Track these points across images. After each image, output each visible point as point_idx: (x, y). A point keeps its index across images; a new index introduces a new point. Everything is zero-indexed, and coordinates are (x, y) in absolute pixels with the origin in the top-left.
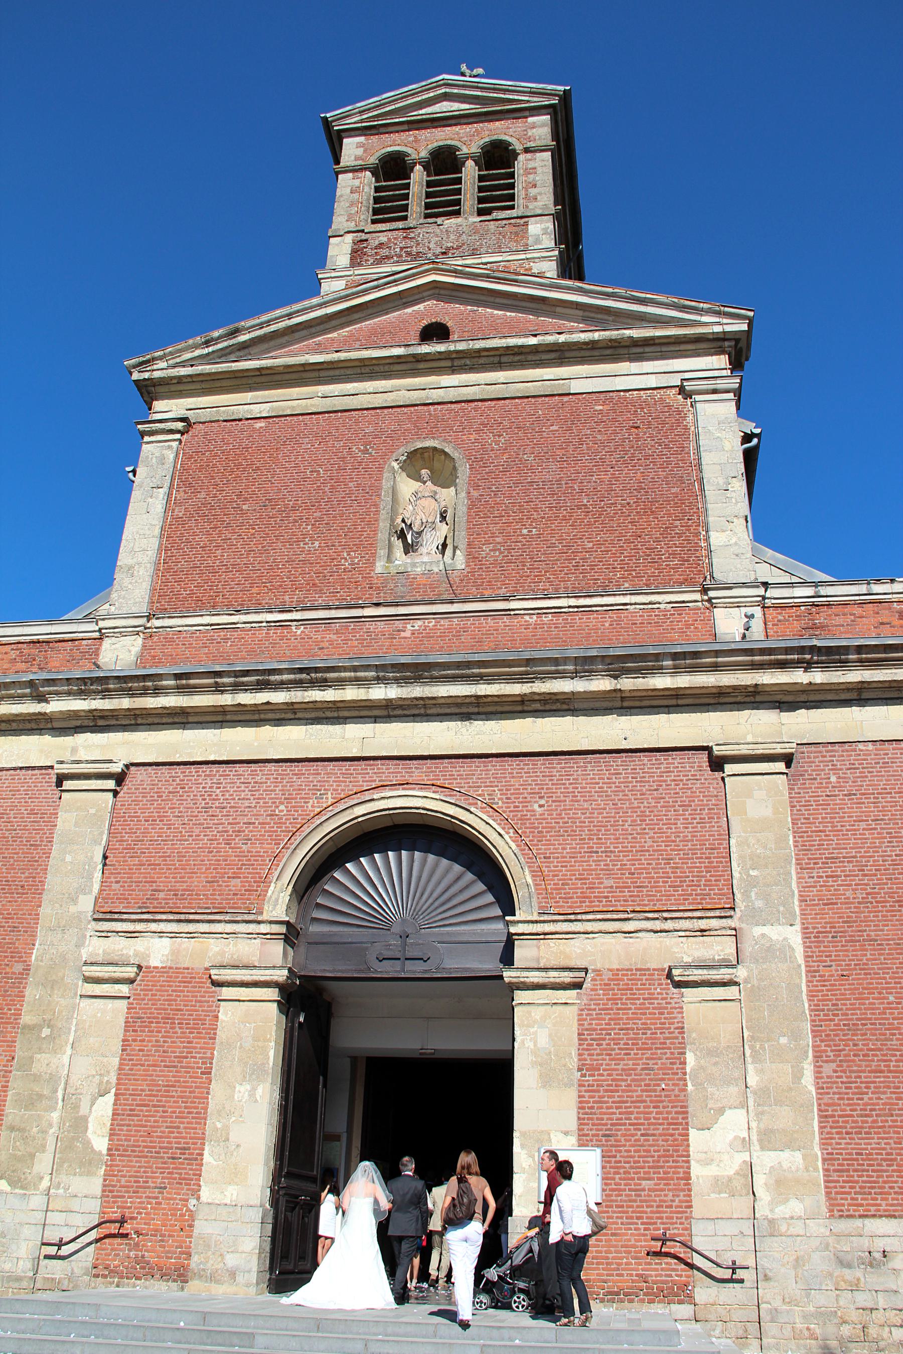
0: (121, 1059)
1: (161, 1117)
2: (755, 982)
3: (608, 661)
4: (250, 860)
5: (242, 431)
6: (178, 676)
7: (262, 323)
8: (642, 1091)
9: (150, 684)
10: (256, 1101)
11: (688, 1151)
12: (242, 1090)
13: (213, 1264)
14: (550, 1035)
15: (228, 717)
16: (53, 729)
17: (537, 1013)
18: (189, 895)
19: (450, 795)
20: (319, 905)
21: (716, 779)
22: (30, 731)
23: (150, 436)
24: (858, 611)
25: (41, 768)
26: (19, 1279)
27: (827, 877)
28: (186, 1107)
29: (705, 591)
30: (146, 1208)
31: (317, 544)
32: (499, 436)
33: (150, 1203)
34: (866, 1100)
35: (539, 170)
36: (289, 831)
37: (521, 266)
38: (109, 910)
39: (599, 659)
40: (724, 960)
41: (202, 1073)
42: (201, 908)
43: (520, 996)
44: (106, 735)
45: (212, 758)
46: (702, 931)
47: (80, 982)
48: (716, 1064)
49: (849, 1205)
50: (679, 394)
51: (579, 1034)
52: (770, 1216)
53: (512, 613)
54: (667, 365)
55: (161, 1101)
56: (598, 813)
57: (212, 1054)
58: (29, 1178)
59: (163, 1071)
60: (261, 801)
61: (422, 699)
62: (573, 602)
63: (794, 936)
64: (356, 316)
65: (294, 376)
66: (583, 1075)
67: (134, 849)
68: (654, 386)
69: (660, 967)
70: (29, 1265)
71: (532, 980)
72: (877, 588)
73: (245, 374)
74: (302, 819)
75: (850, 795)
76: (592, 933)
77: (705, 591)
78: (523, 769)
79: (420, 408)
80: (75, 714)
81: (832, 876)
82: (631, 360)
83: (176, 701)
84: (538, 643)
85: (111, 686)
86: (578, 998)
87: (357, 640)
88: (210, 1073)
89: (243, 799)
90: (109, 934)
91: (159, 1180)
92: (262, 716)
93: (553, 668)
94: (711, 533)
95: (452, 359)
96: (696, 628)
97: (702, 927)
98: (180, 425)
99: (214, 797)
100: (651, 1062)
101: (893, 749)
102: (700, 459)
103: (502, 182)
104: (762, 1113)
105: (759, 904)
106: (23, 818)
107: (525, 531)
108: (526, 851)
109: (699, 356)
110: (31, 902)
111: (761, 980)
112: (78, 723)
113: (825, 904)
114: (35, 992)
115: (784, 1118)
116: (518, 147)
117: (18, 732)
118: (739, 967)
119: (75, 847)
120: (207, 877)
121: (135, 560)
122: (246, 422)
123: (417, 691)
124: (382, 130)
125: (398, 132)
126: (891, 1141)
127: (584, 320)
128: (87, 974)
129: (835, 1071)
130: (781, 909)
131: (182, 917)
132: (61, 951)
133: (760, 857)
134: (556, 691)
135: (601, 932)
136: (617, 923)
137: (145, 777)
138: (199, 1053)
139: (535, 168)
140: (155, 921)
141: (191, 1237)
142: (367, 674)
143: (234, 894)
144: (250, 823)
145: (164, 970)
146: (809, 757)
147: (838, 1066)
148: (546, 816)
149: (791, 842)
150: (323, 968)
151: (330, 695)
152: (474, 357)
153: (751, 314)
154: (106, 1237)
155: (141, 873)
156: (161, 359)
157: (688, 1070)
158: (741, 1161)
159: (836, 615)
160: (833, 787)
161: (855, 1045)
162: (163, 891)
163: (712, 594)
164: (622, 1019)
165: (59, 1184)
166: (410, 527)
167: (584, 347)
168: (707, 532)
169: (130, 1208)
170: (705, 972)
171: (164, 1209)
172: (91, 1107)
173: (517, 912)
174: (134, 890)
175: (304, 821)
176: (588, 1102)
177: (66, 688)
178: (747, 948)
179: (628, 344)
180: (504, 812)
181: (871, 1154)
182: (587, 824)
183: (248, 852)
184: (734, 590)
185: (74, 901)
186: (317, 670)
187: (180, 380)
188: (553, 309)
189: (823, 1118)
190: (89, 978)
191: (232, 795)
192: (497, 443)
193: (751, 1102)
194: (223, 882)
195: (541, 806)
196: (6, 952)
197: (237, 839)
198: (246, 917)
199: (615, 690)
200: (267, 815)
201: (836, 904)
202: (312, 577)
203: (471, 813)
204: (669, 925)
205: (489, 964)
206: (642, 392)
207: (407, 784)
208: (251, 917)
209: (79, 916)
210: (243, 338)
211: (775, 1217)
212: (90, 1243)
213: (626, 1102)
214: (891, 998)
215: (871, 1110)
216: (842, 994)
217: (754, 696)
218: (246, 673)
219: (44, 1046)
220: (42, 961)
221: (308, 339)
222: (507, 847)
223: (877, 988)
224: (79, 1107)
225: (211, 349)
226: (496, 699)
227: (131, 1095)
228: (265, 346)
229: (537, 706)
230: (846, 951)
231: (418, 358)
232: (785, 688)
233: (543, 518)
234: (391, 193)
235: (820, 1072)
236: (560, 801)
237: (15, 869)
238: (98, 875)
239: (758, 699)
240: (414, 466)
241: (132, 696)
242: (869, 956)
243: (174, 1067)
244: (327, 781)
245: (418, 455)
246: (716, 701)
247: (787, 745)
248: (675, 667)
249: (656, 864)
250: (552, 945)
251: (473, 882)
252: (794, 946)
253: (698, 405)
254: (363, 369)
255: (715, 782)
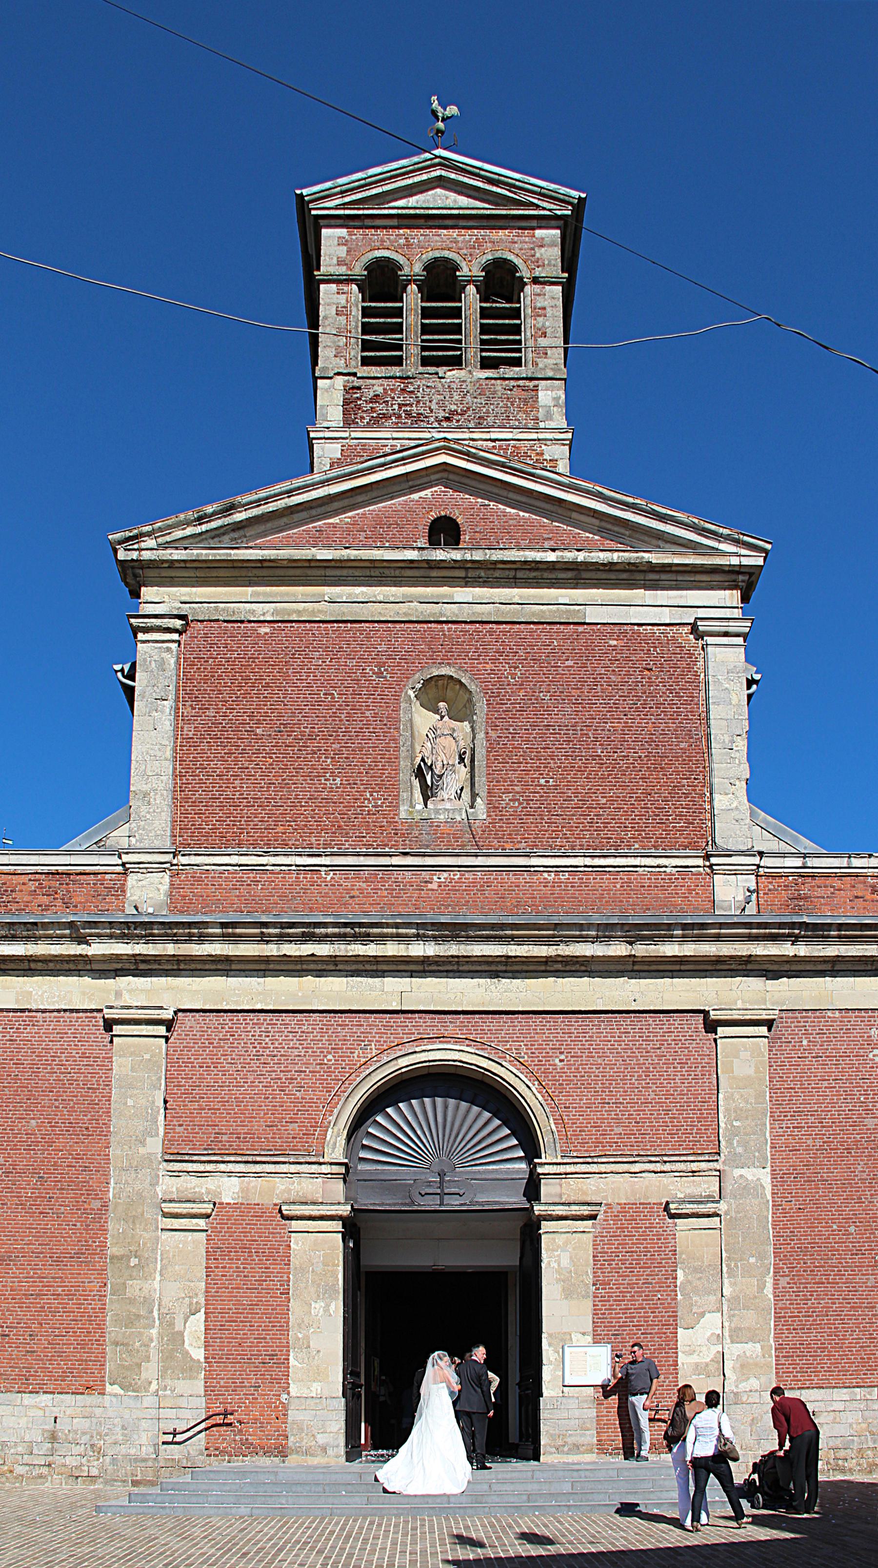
0: (206, 1284)
1: (249, 1330)
2: (733, 1214)
3: (626, 928)
4: (304, 1106)
5: (245, 636)
6: (223, 925)
7: (259, 500)
8: (643, 1300)
9: (196, 931)
10: (330, 1315)
11: (676, 1345)
12: (318, 1307)
13: (306, 1442)
14: (571, 1258)
15: (271, 966)
16: (92, 970)
17: (560, 1239)
18: (250, 1138)
19: (482, 1049)
20: (364, 1147)
21: (709, 1040)
22: (68, 973)
23: (144, 632)
24: (837, 883)
25: (85, 1011)
26: (145, 1460)
27: (794, 1127)
28: (270, 1322)
29: (707, 857)
30: (245, 1403)
31: (338, 780)
32: (515, 668)
33: (248, 1399)
34: (809, 1304)
35: (549, 312)
36: (339, 1080)
37: (531, 449)
38: (176, 1151)
39: (619, 926)
40: (709, 1196)
41: (281, 1293)
42: (264, 1150)
43: (546, 1226)
44: (149, 979)
45: (258, 1007)
46: (693, 1172)
47: (160, 1217)
48: (700, 1279)
49: (792, 1380)
50: (691, 633)
51: (594, 1256)
52: (735, 1390)
53: (532, 869)
54: (681, 597)
55: (247, 1317)
56: (610, 1069)
57: (288, 1277)
58: (139, 1383)
59: (246, 1293)
60: (310, 1050)
61: (458, 957)
62: (588, 861)
63: (765, 1177)
64: (360, 499)
65: (298, 572)
66: (598, 1289)
67: (192, 1094)
68: (668, 621)
69: (659, 1201)
70: (152, 1450)
71: (557, 1213)
72: (856, 862)
73: (245, 565)
74: (350, 1068)
75: (817, 1057)
76: (605, 1173)
77: (707, 857)
78: (545, 1026)
79: (433, 625)
80: (117, 958)
81: (797, 1127)
82: (646, 588)
83: (222, 949)
84: (556, 902)
85: (156, 931)
86: (593, 1228)
87: (386, 889)
88: (288, 1293)
89: (293, 1048)
90: (181, 1174)
91: (253, 1381)
92: (305, 967)
93: (578, 933)
94: (716, 796)
95: (467, 569)
96: (697, 893)
97: (694, 1169)
98: (178, 623)
99: (263, 1045)
100: (650, 1278)
101: (856, 1017)
102: (708, 712)
103: (507, 322)
104: (733, 1316)
105: (740, 1150)
106: (75, 1061)
107: (542, 781)
108: (549, 1102)
109: (712, 588)
110: (98, 1143)
111: (738, 1212)
112: (119, 966)
113: (790, 1151)
114: (117, 1226)
115: (750, 1318)
116: (525, 273)
117: (55, 973)
118: (722, 1202)
119: (136, 1092)
120: (266, 1122)
121: (149, 785)
122: (249, 625)
123: (453, 949)
124: (368, 222)
125: (385, 227)
126: (825, 1334)
127: (599, 531)
128: (165, 1210)
129: (789, 1283)
130: (757, 1154)
131: (250, 1159)
132: (136, 1189)
133: (742, 1110)
134: (578, 954)
135: (612, 1172)
136: (626, 1165)
137: (193, 1023)
138: (277, 1277)
139: (544, 308)
140: (223, 1162)
141: (286, 1423)
142: (408, 931)
143: (293, 1138)
144: (301, 1071)
145: (236, 1206)
146: (786, 1022)
147: (791, 1279)
148: (566, 1070)
149: (768, 1098)
150: (372, 1202)
151: (371, 950)
152: (489, 569)
153: (769, 547)
154: (213, 1426)
155: (202, 1117)
156: (149, 536)
157: (678, 1284)
158: (715, 1352)
159: (819, 887)
160: (804, 1050)
161: (805, 1263)
162: (226, 1134)
163: (714, 860)
164: (628, 1244)
165: (166, 1387)
166: (430, 768)
167: (602, 568)
168: (711, 794)
169: (230, 1403)
170: (696, 1206)
171: (260, 1403)
172: (185, 1323)
173: (543, 1155)
174: (198, 1133)
175: (352, 1071)
176: (601, 1310)
177: (108, 931)
178: (728, 1187)
179: (645, 568)
180: (530, 1065)
181: (810, 1344)
182: (600, 1078)
183: (303, 1098)
184: (733, 858)
185: (143, 1143)
186: (361, 925)
187: (172, 564)
188: (569, 513)
189: (777, 1318)
190: (167, 1213)
191: (281, 1044)
192: (513, 676)
193: (725, 1308)
194: (282, 1126)
195: (561, 1061)
196: (81, 1190)
197: (291, 1086)
198: (308, 1159)
199: (630, 956)
200: (317, 1064)
201: (799, 1150)
202: (336, 818)
203: (502, 1066)
204: (667, 1167)
205: (515, 1199)
206: (655, 628)
207: (443, 1037)
208: (314, 1159)
209: (149, 1156)
210: (240, 516)
211: (739, 1390)
212: (201, 1432)
213: (630, 1309)
214: (835, 1227)
215: (813, 1312)
216: (798, 1224)
217: (746, 964)
218: (292, 925)
219: (134, 1274)
220: (119, 1198)
221: (307, 524)
222: (534, 1098)
223: (824, 1219)
224: (174, 1324)
225: (204, 528)
226: (524, 959)
227: (219, 1313)
228: (262, 528)
229: (559, 967)
230: (804, 1189)
231: (432, 565)
232: (773, 958)
233: (559, 767)
234: (382, 320)
235: (778, 1284)
236: (577, 1057)
237: (76, 1111)
238: (161, 1118)
239: (749, 967)
240: (427, 694)
241: (176, 942)
242: (821, 1193)
243: (256, 1289)
244: (370, 1033)
245: (433, 683)
246: (713, 968)
247: (771, 1012)
248: (683, 936)
249: (658, 1114)
250: (572, 1183)
251: (499, 1127)
252: (765, 1185)
253: (710, 649)
254: (372, 570)
255: (708, 1042)
